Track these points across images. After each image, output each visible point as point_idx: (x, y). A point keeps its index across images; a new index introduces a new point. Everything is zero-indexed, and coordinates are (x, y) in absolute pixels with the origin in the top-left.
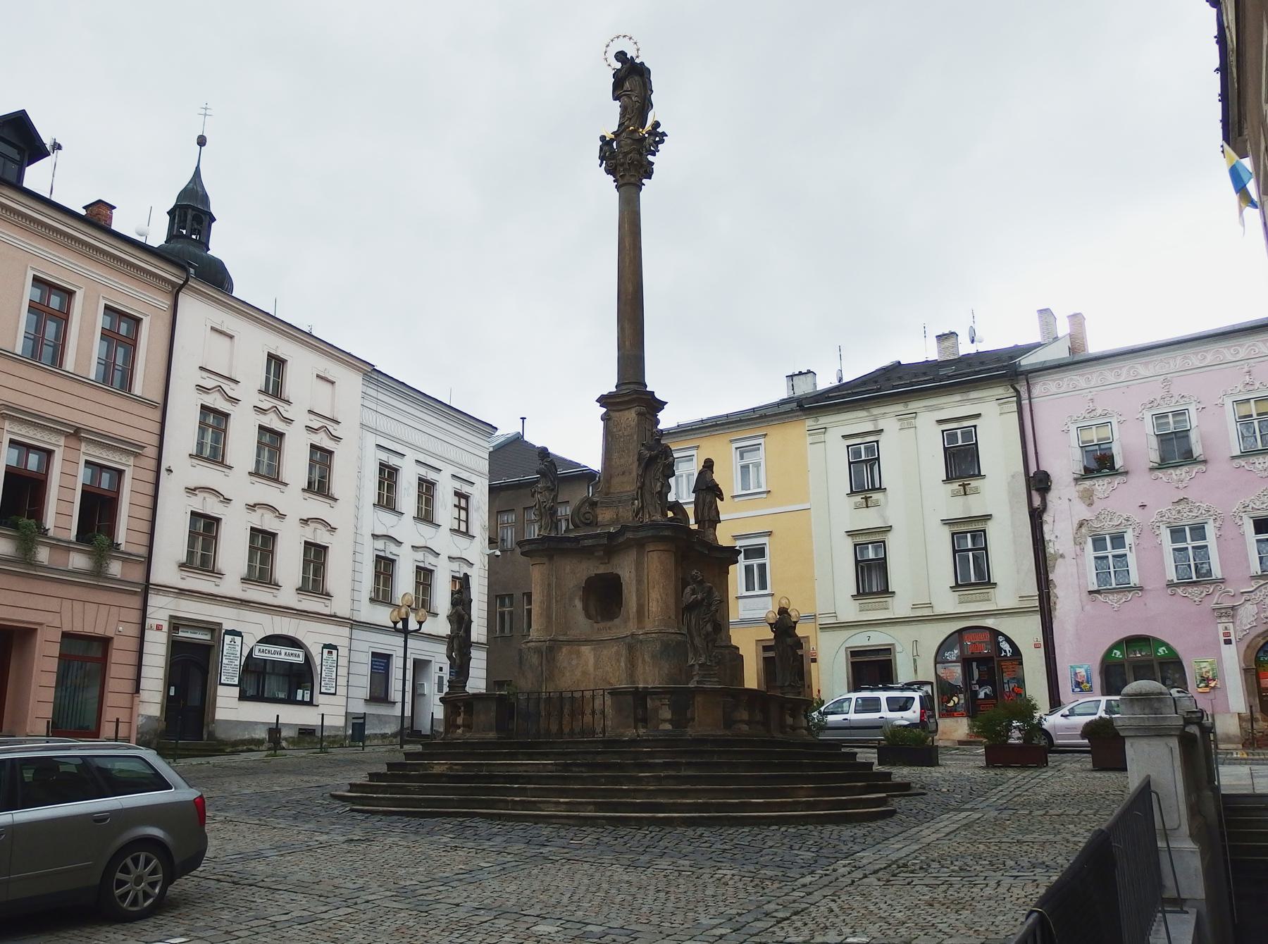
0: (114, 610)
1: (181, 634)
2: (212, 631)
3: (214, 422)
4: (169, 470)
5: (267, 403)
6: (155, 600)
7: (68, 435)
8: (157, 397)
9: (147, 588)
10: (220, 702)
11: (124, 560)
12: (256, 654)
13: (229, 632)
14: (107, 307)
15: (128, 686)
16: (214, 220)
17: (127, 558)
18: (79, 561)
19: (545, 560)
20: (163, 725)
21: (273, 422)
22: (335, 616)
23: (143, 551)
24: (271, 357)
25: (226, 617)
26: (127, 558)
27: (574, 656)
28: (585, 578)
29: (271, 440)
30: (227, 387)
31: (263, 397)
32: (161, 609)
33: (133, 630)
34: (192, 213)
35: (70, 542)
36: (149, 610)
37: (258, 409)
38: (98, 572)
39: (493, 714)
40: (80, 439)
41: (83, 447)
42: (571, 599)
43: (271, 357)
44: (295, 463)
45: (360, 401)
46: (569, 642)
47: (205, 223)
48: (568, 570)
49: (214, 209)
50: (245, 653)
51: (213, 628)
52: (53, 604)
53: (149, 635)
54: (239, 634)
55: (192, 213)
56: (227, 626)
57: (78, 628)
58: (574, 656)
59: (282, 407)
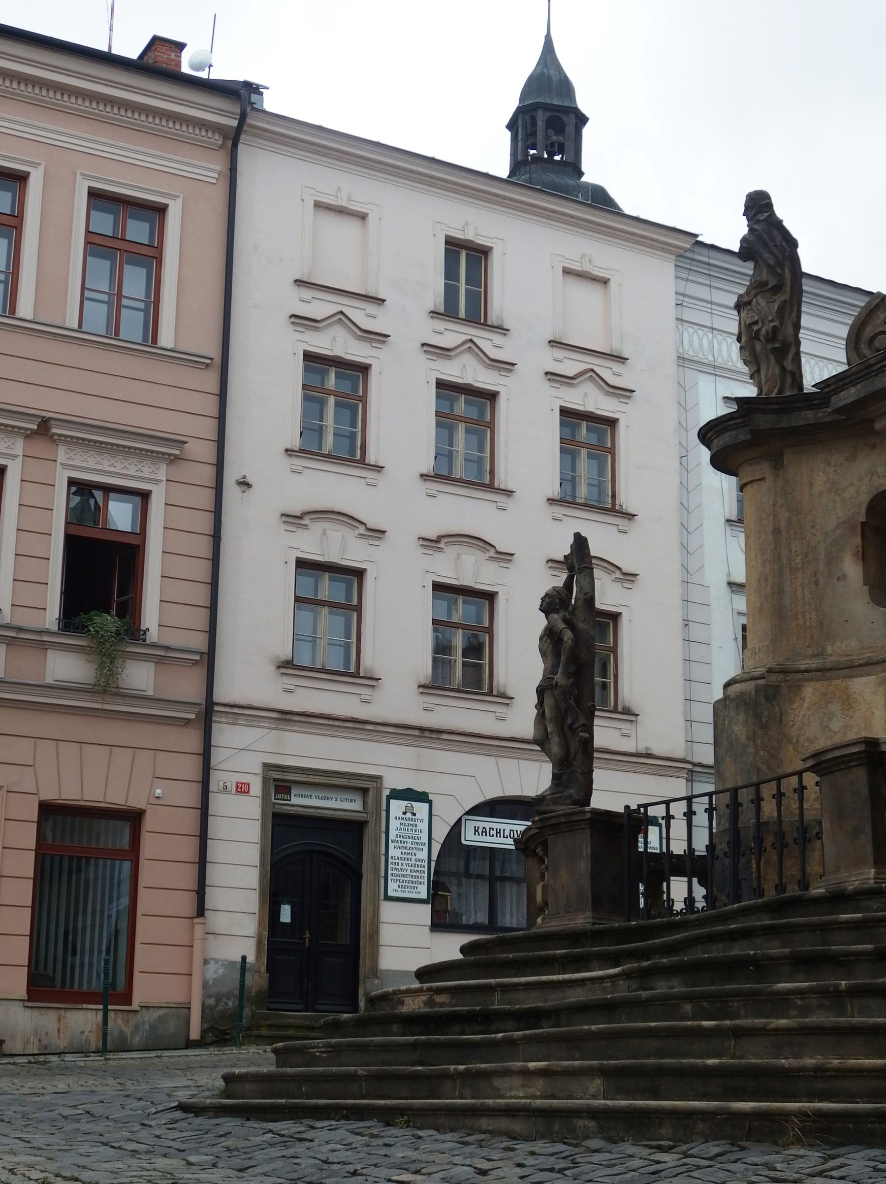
0: (144, 757)
1: (295, 800)
2: (365, 791)
3: (336, 387)
4: (245, 484)
5: (452, 335)
6: (228, 737)
7: (29, 435)
8: (213, 350)
9: (208, 713)
10: (387, 934)
11: (160, 661)
12: (469, 837)
13: (397, 794)
14: (93, 194)
15: (186, 903)
16: (582, 120)
17: (164, 657)
18: (66, 666)
19: (764, 469)
20: (257, 981)
21: (466, 371)
22: (649, 756)
23: (199, 642)
24: (454, 246)
25: (393, 765)
26: (164, 657)
27: (835, 707)
28: (865, 499)
29: (467, 410)
30: (359, 314)
31: (440, 325)
32: (243, 753)
33: (189, 795)
34: (548, 121)
35: (48, 632)
36: (217, 756)
37: (432, 350)
38: (106, 686)
39: (584, 866)
40: (54, 440)
41: (62, 454)
42: (832, 560)
43: (454, 246)
44: (528, 445)
45: (671, 312)
46: (825, 672)
47: (570, 129)
48: (820, 480)
49: (583, 104)
50: (441, 833)
51: (364, 786)
52: (21, 750)
53: (220, 804)
54: (423, 797)
55: (548, 121)
56: (393, 781)
57: (70, 792)
58: (835, 707)
59: (487, 341)
